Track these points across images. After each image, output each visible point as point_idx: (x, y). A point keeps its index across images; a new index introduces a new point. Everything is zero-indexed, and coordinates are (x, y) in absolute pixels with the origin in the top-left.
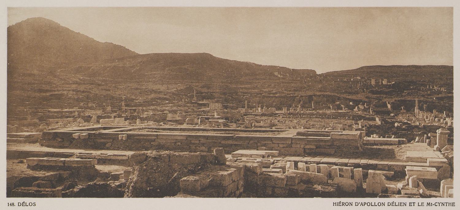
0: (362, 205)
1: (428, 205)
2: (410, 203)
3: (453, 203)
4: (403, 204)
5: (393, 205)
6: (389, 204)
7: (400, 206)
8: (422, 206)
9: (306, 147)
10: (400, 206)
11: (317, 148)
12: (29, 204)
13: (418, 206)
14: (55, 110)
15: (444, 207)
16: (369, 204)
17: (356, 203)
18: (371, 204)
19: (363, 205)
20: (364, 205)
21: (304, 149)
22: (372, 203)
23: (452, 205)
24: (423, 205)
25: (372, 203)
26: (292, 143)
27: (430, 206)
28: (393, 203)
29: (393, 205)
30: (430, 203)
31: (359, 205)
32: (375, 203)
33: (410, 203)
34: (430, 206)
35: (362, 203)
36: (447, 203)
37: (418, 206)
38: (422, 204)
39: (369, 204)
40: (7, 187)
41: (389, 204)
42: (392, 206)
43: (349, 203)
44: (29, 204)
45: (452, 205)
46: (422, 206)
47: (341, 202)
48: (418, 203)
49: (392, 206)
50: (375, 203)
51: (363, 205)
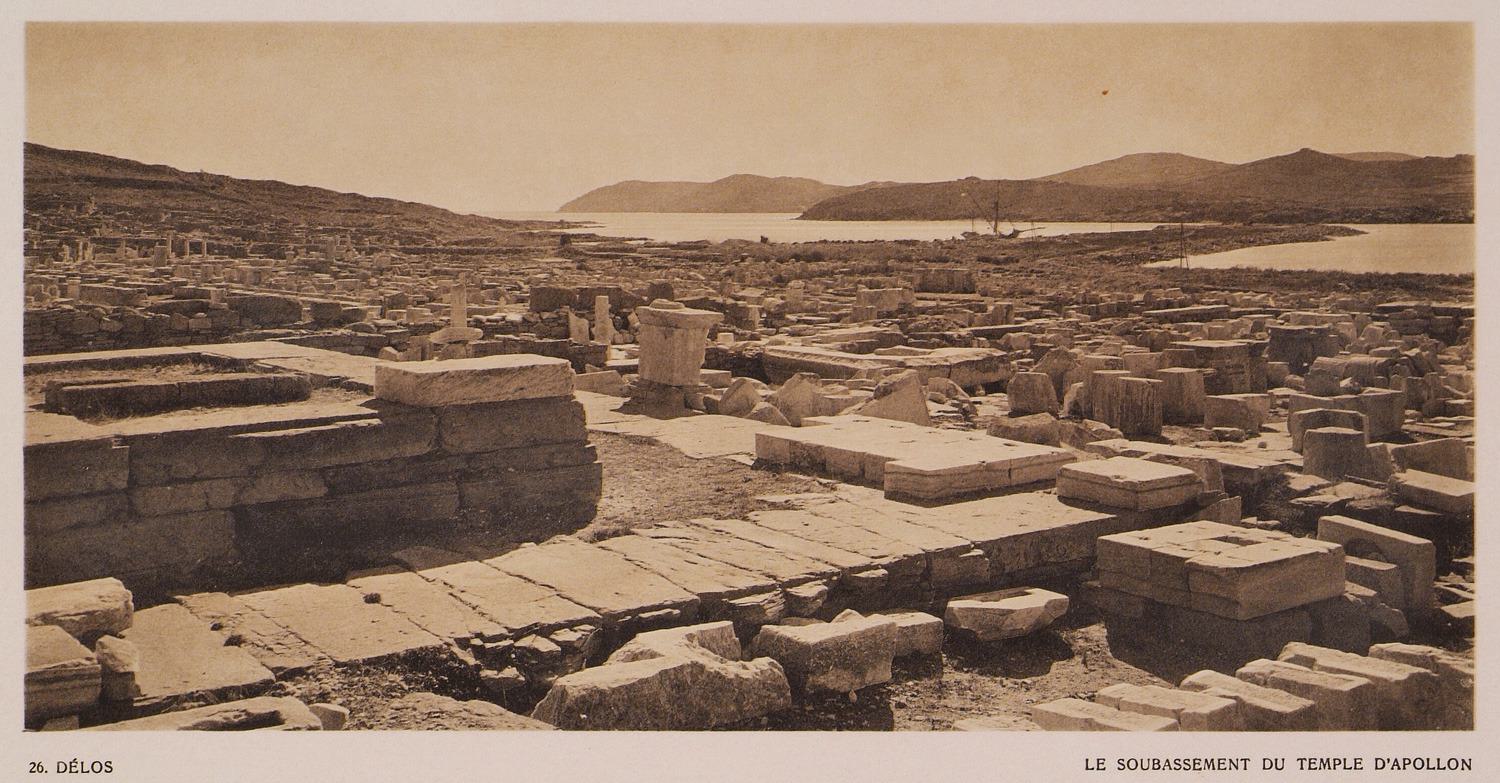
0: (1396, 767)
1: (1325, 765)
2: (1098, 760)
3: (1335, 760)
4: (1227, 762)
5: (74, 769)
6: (62, 768)
7: (1219, 769)
8: (1355, 768)
9: (252, 497)
10: (1219, 769)
11: (333, 491)
12: (1449, 764)
13: (1087, 768)
14: (1344, 396)
15: (1324, 774)
16: (1419, 764)
17: (1377, 760)
18: (1426, 764)
19: (1399, 768)
20: (1404, 768)
21: (239, 511)
22: (1428, 760)
23: (1216, 767)
24: (1101, 767)
25: (1428, 760)
26: (133, 482)
27: (1329, 768)
28: (73, 764)
29: (74, 769)
30: (1212, 760)
31: (1388, 766)
32: (1438, 760)
33: (1098, 760)
34: (1329, 768)
35: (1396, 760)
36: (1302, 760)
37: (1087, 768)
38: (1098, 764)
39: (1419, 764)
40: (1348, 730)
41: (62, 768)
42: (71, 772)
43: (1460, 763)
44: (1449, 764)
45: (1216, 767)
46: (1355, 768)
47: (79, 761)
48: (1087, 760)
49: (71, 772)
50: (1438, 760)
51: (1402, 767)
